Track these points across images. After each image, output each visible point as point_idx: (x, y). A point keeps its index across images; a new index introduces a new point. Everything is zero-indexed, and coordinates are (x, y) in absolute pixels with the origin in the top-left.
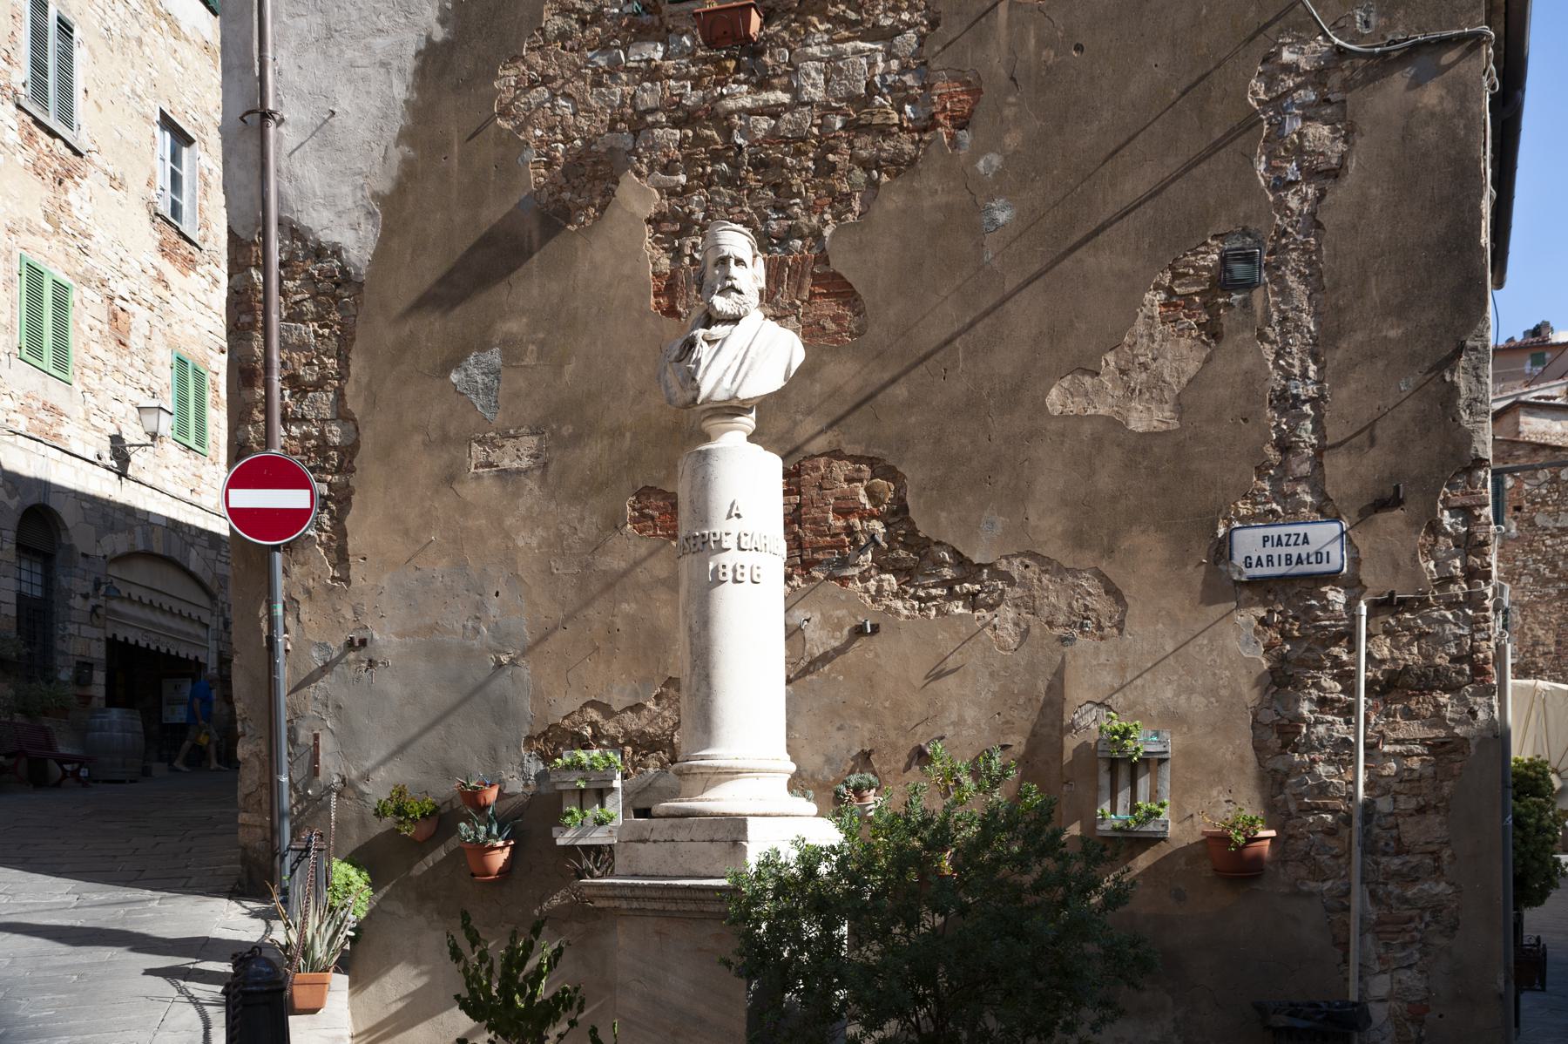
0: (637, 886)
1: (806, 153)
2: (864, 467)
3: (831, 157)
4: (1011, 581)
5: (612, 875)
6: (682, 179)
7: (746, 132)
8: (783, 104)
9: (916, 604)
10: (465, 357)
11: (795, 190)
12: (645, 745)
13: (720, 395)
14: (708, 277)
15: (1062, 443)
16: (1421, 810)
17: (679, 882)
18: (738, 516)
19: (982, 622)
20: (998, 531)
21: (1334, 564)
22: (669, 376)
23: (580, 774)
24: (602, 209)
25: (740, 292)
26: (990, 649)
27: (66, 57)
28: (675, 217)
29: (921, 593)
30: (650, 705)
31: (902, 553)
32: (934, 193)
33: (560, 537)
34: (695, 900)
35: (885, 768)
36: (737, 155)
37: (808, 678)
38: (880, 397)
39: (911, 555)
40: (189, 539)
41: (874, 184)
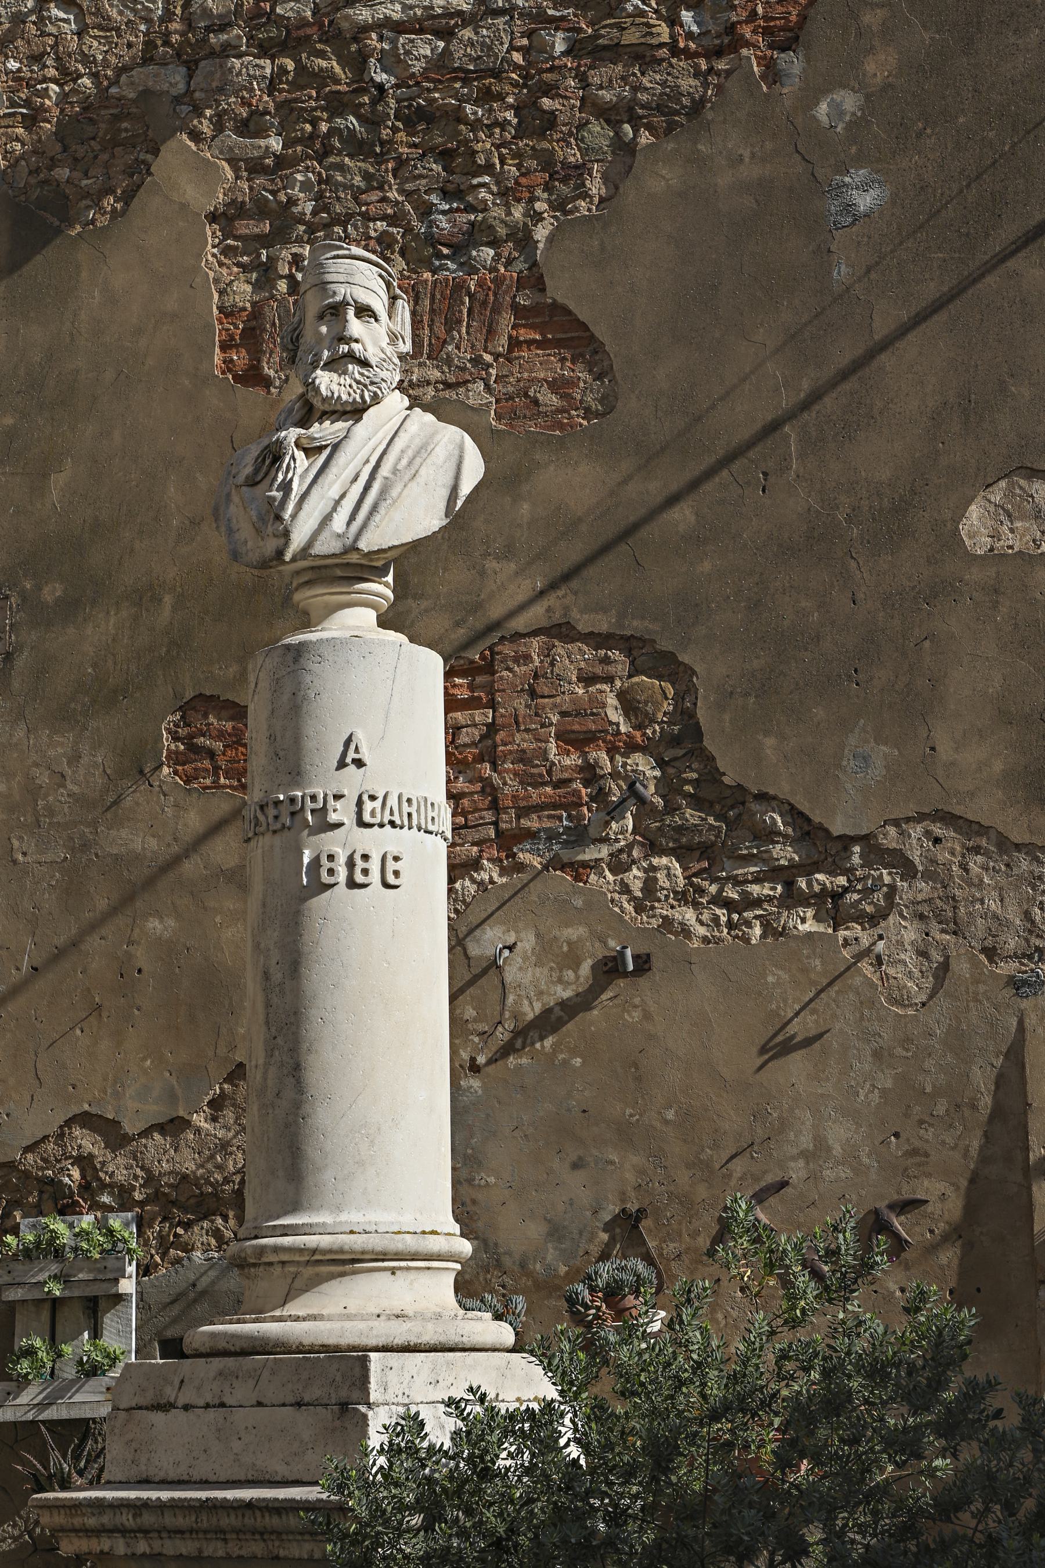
0: (146, 1505)
1: (501, 97)
2: (615, 654)
3: (546, 103)
4: (908, 870)
5: (95, 1483)
6: (276, 144)
7: (391, 61)
8: (460, 13)
9: (722, 913)
11: (481, 160)
12: (180, 1204)
13: (326, 546)
14: (308, 337)
15: (995, 605)
17: (230, 1494)
18: (359, 763)
19: (855, 949)
20: (877, 770)
22: (234, 510)
23: (54, 1268)
24: (128, 198)
25: (365, 363)
26: (872, 1003)
28: (261, 209)
29: (732, 893)
30: (199, 1120)
31: (691, 816)
33: (32, 791)
34: (262, 1533)
35: (671, 1248)
36: (374, 102)
37: (512, 1061)
38: (644, 533)
39: (712, 818)
41: (625, 149)
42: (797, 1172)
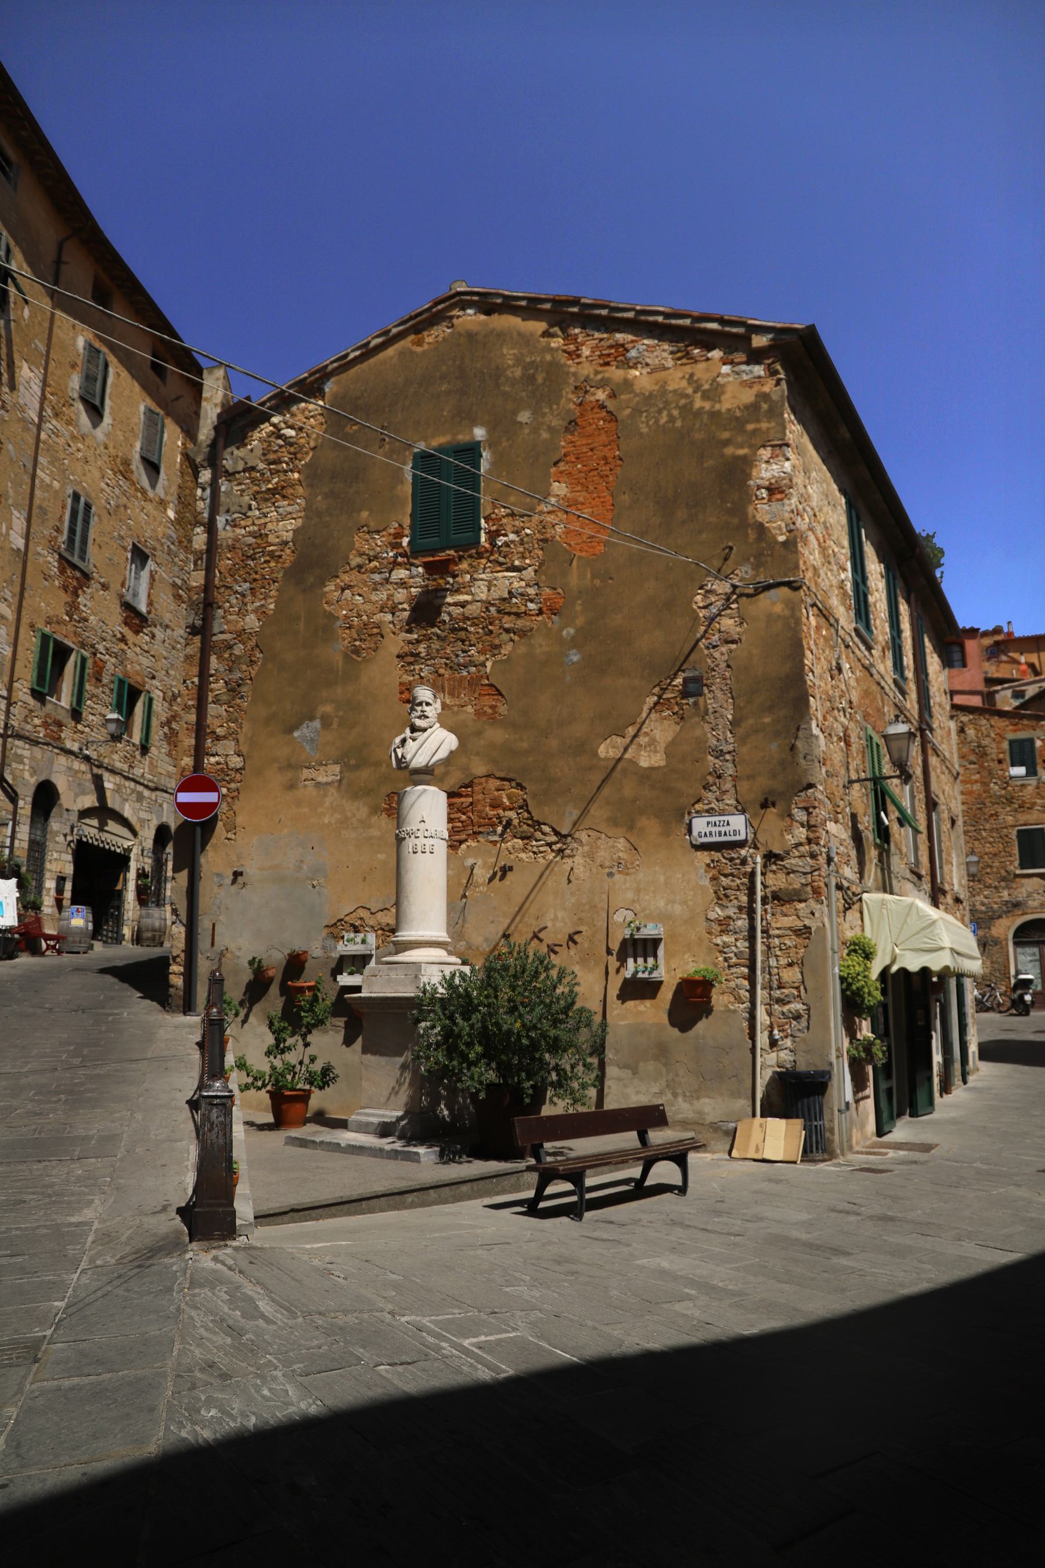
10: (301, 724)
16: (790, 965)
21: (742, 837)
27: (86, 522)
28: (412, 655)
32: (541, 646)
40: (125, 797)
42: (549, 924)
